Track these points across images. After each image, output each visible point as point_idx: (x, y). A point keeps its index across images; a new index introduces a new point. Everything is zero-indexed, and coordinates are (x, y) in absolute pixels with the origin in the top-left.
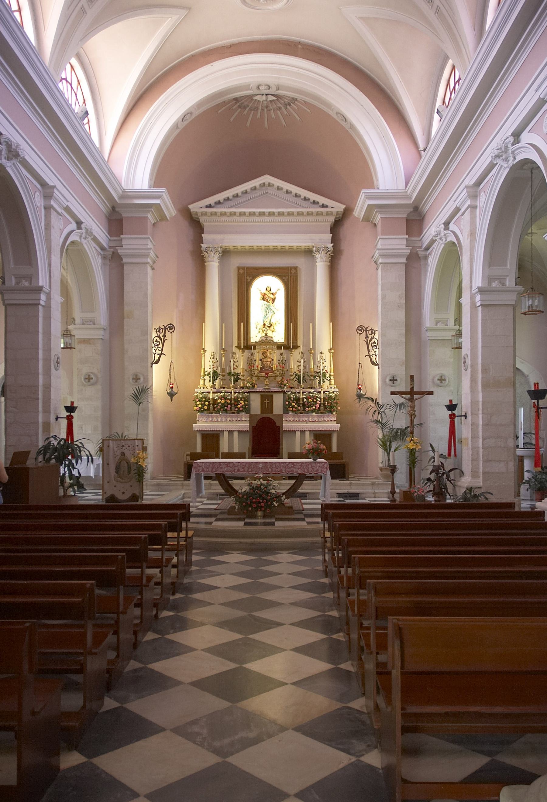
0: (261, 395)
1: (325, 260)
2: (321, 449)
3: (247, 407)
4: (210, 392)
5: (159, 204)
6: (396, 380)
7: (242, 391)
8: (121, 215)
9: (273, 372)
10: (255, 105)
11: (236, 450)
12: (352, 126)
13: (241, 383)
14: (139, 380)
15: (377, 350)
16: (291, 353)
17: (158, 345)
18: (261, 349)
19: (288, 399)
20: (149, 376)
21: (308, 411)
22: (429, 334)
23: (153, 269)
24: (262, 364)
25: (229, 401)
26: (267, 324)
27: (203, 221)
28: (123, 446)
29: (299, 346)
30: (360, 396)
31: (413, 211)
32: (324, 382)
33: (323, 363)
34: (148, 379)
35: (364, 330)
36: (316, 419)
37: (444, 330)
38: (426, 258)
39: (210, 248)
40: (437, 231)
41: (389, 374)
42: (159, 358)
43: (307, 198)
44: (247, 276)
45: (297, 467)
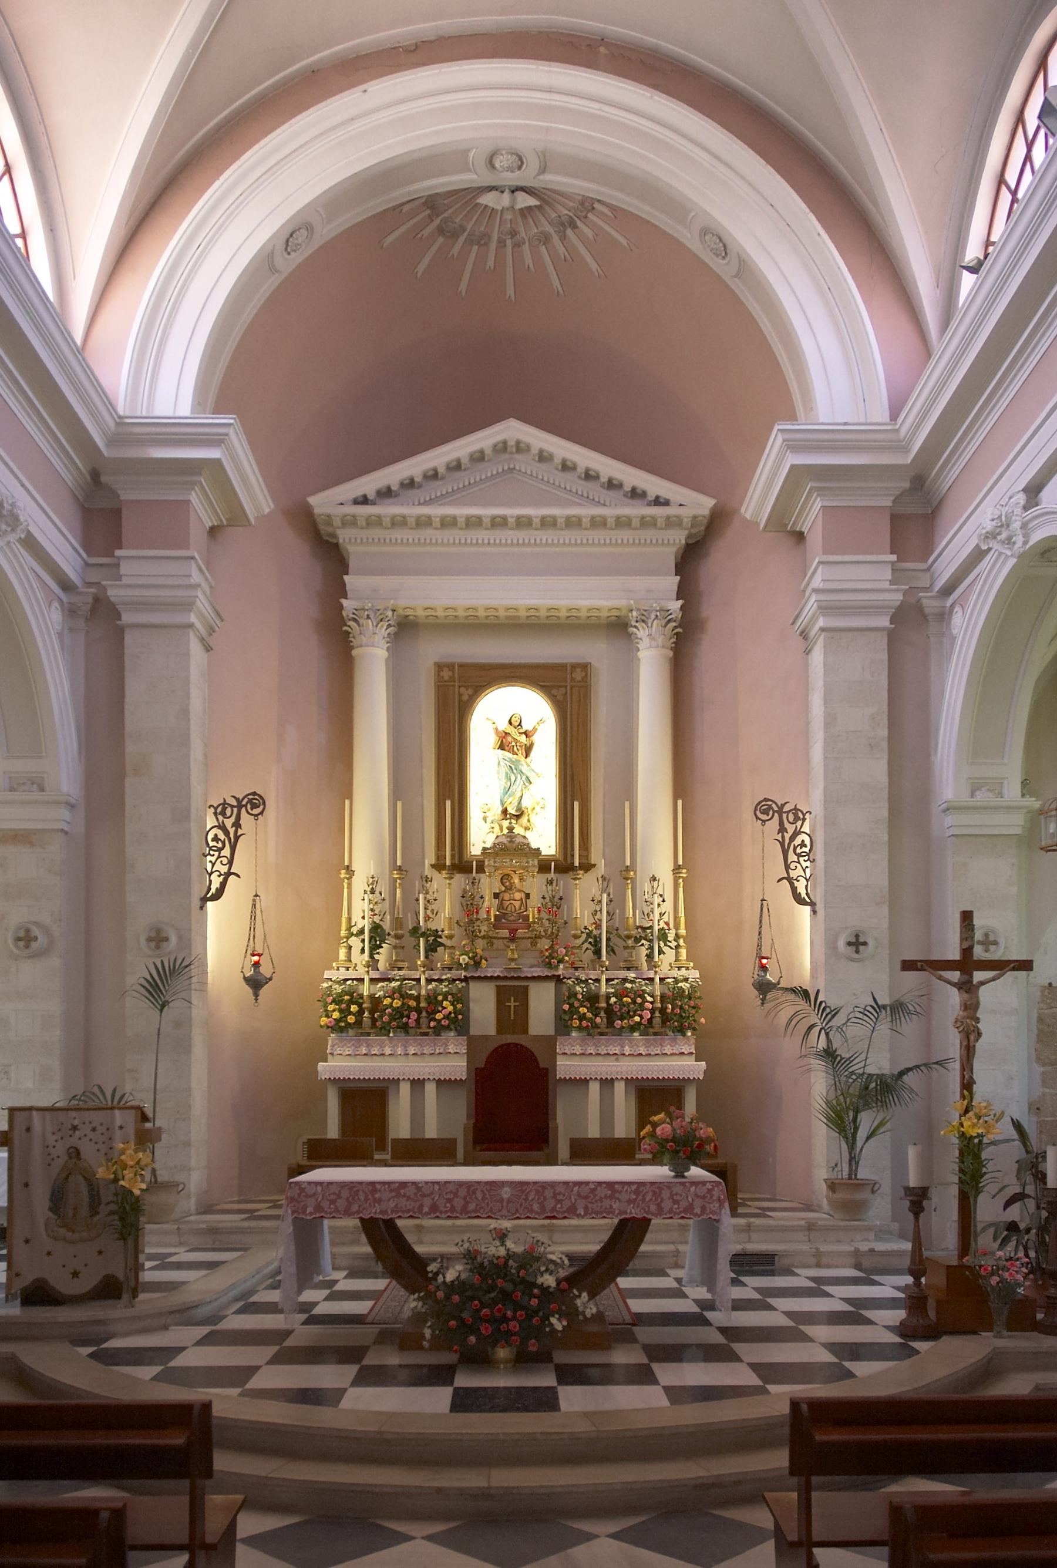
0: (497, 986)
1: (660, 643)
2: (701, 1139)
3: (460, 1017)
4: (362, 980)
5: (218, 462)
6: (865, 944)
7: (449, 975)
8: (118, 496)
9: (528, 926)
10: (482, 229)
11: (431, 1132)
12: (745, 268)
13: (443, 956)
14: (165, 944)
15: (808, 864)
16: (575, 879)
17: (220, 850)
18: (496, 869)
19: (569, 998)
20: (193, 933)
21: (623, 1027)
22: (949, 820)
23: (208, 649)
24: (500, 906)
25: (413, 1003)
26: (512, 810)
27: (347, 540)
28: (75, 1128)
29: (594, 865)
30: (764, 988)
31: (910, 489)
32: (661, 952)
33: (659, 905)
34: (190, 940)
35: (774, 812)
36: (642, 1051)
37: (995, 809)
38: (944, 616)
39: (364, 609)
40: (1000, 517)
41: (846, 928)
42: (223, 885)
43: (615, 482)
44: (460, 687)
45: (624, 1197)
